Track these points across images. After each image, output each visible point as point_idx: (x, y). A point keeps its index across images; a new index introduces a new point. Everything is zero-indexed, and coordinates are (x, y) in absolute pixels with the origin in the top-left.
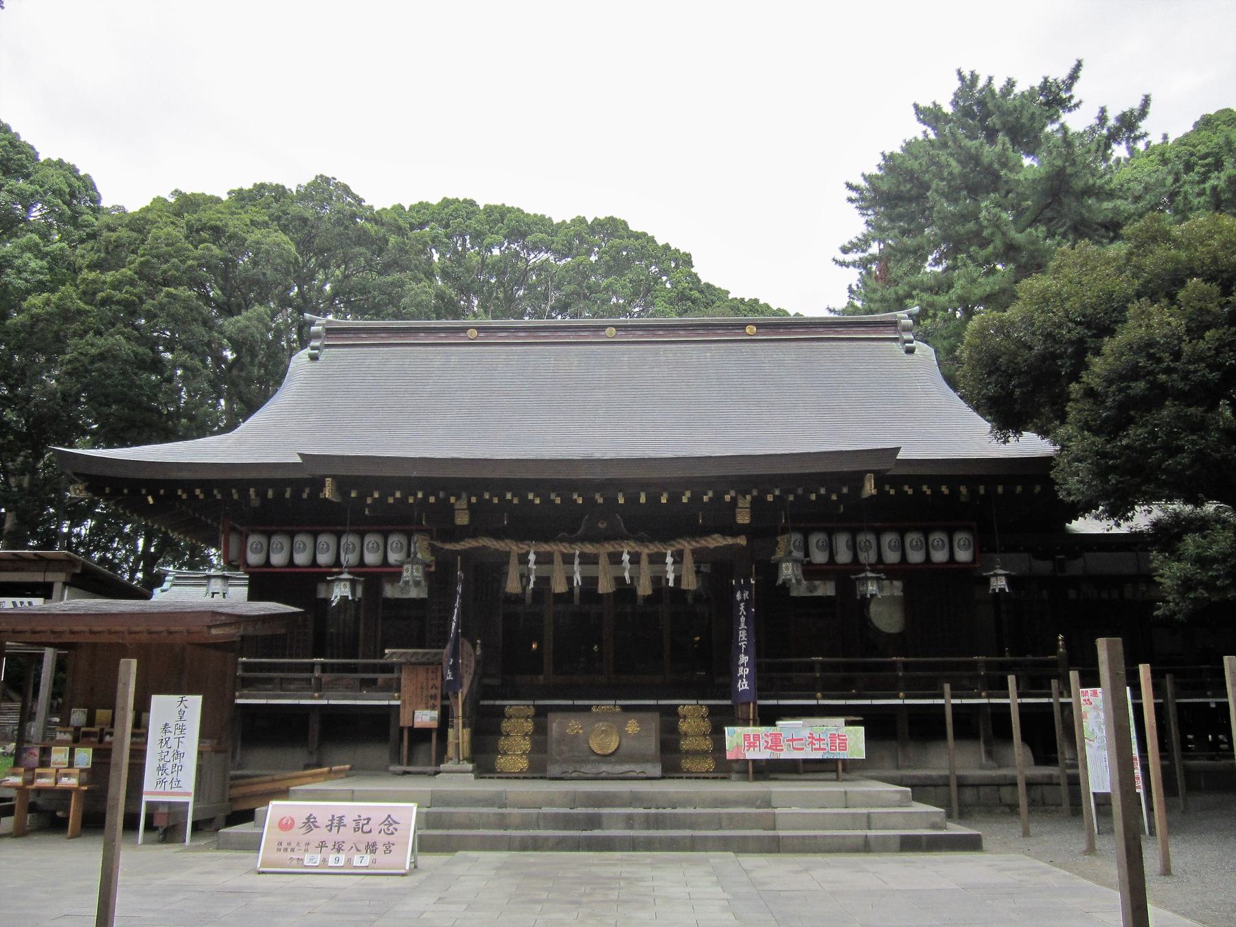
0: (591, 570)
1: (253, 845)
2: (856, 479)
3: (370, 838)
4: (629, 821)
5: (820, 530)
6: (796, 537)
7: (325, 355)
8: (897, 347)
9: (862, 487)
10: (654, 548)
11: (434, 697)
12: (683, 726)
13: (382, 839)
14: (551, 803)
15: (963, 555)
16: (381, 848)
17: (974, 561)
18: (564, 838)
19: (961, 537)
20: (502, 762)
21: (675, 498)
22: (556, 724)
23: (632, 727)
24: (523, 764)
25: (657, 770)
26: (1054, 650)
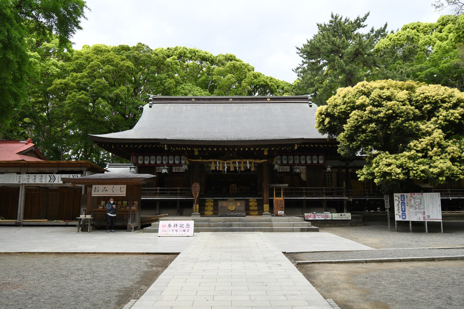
0: (229, 165)
1: (157, 231)
2: (293, 145)
3: (184, 229)
4: (239, 225)
5: (285, 155)
6: (279, 157)
7: (154, 106)
8: (307, 105)
9: (294, 147)
10: (245, 160)
11: (282, 207)
12: (250, 204)
13: (186, 229)
14: (221, 221)
15: (321, 162)
16: (186, 231)
17: (324, 163)
18: (224, 229)
19: (321, 157)
20: (206, 213)
21: (249, 149)
22: (220, 204)
23: (239, 204)
24: (211, 213)
25: (244, 214)
26: (342, 186)
